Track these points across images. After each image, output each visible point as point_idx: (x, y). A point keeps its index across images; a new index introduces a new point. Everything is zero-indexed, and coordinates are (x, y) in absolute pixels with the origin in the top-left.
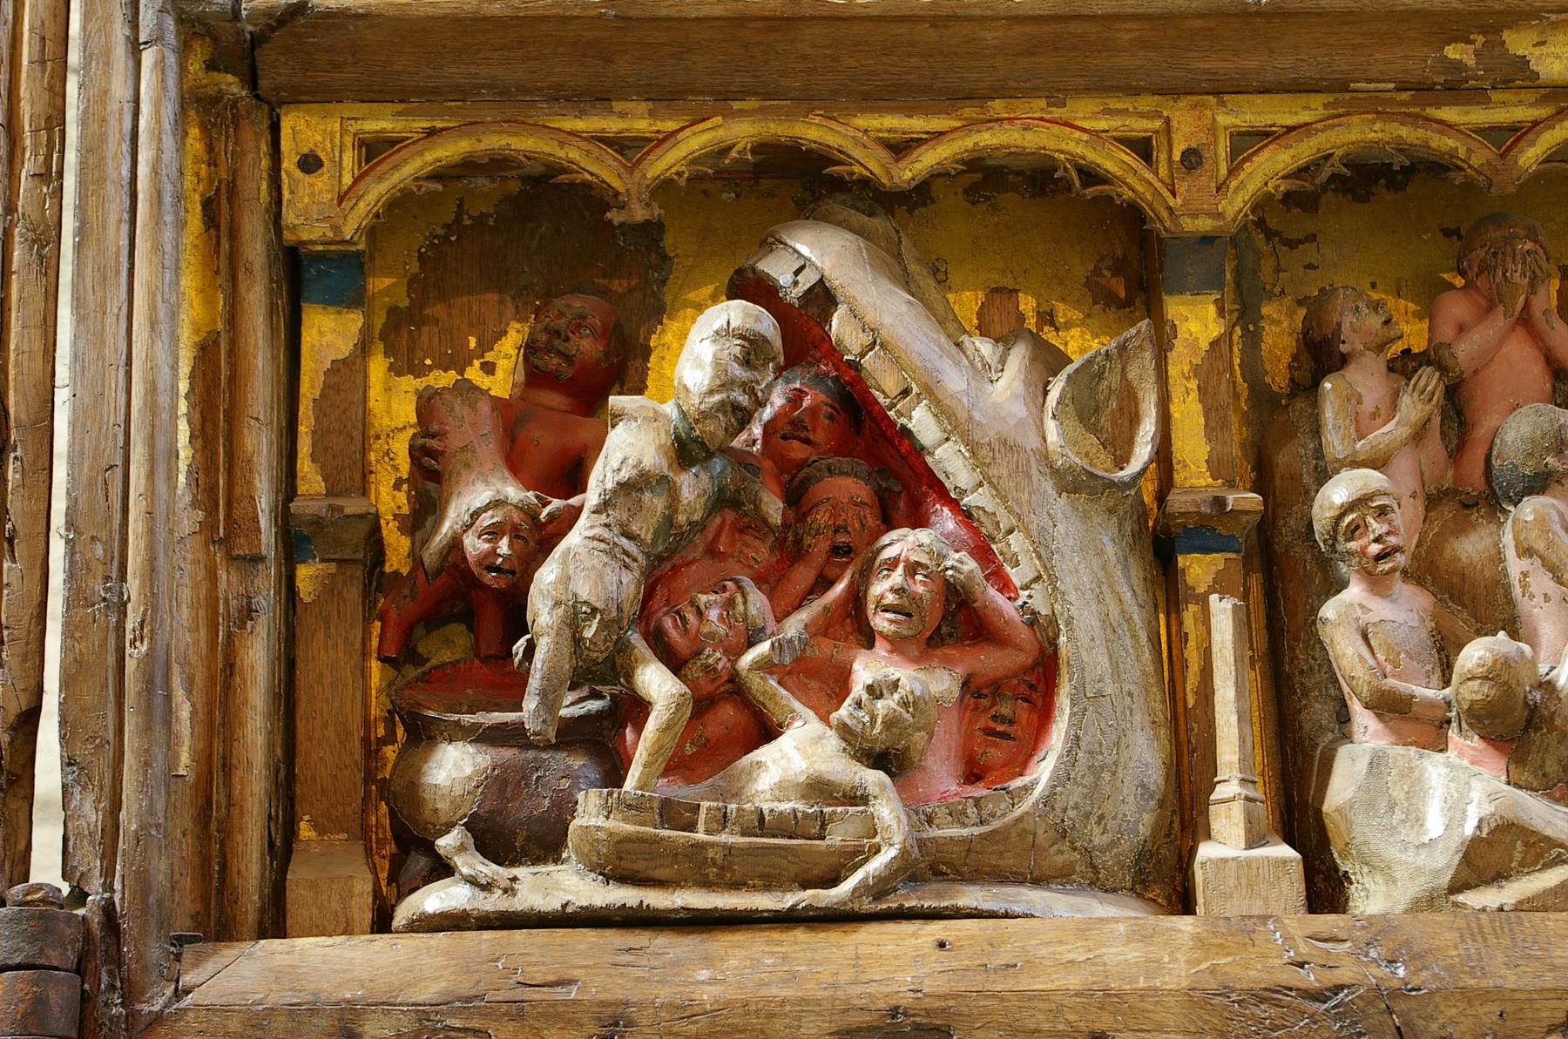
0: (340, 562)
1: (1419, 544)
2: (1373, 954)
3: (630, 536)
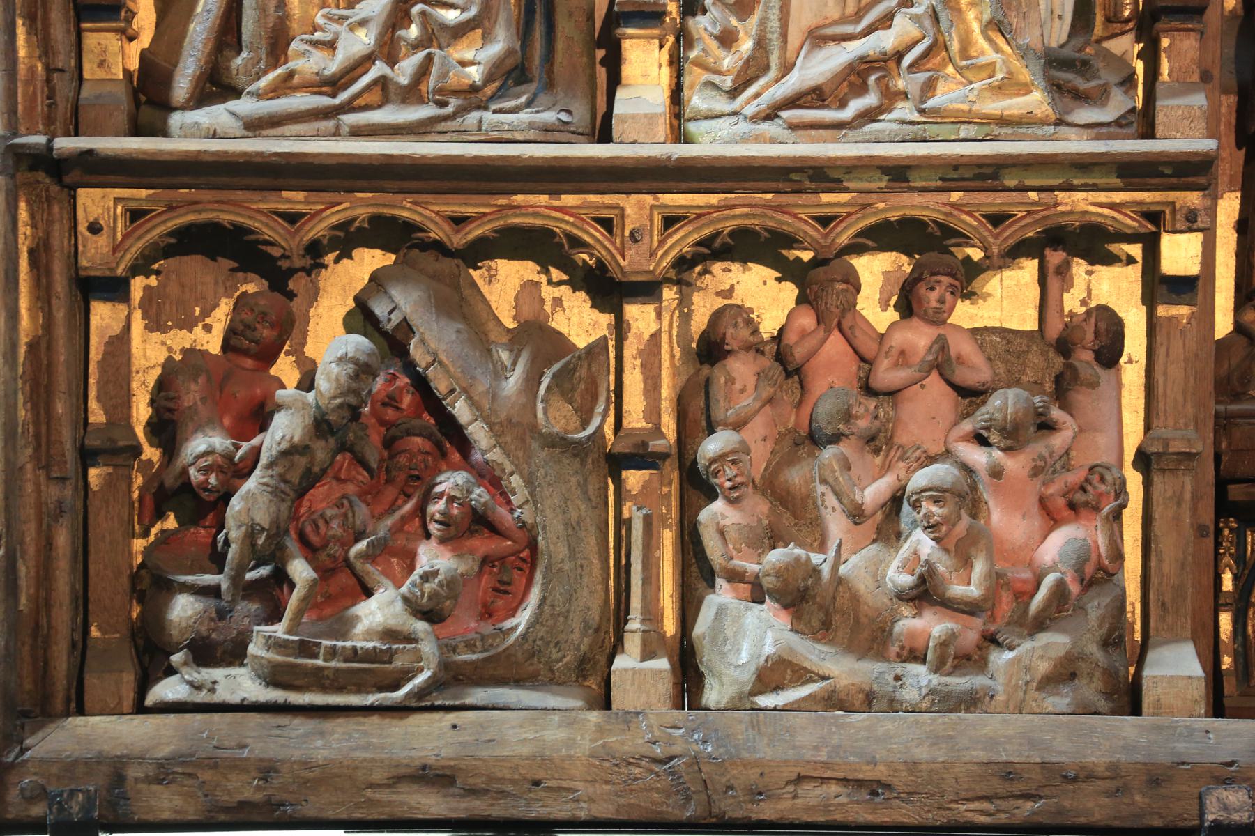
0: (115, 466)
1: (766, 469)
2: (696, 736)
3: (286, 482)
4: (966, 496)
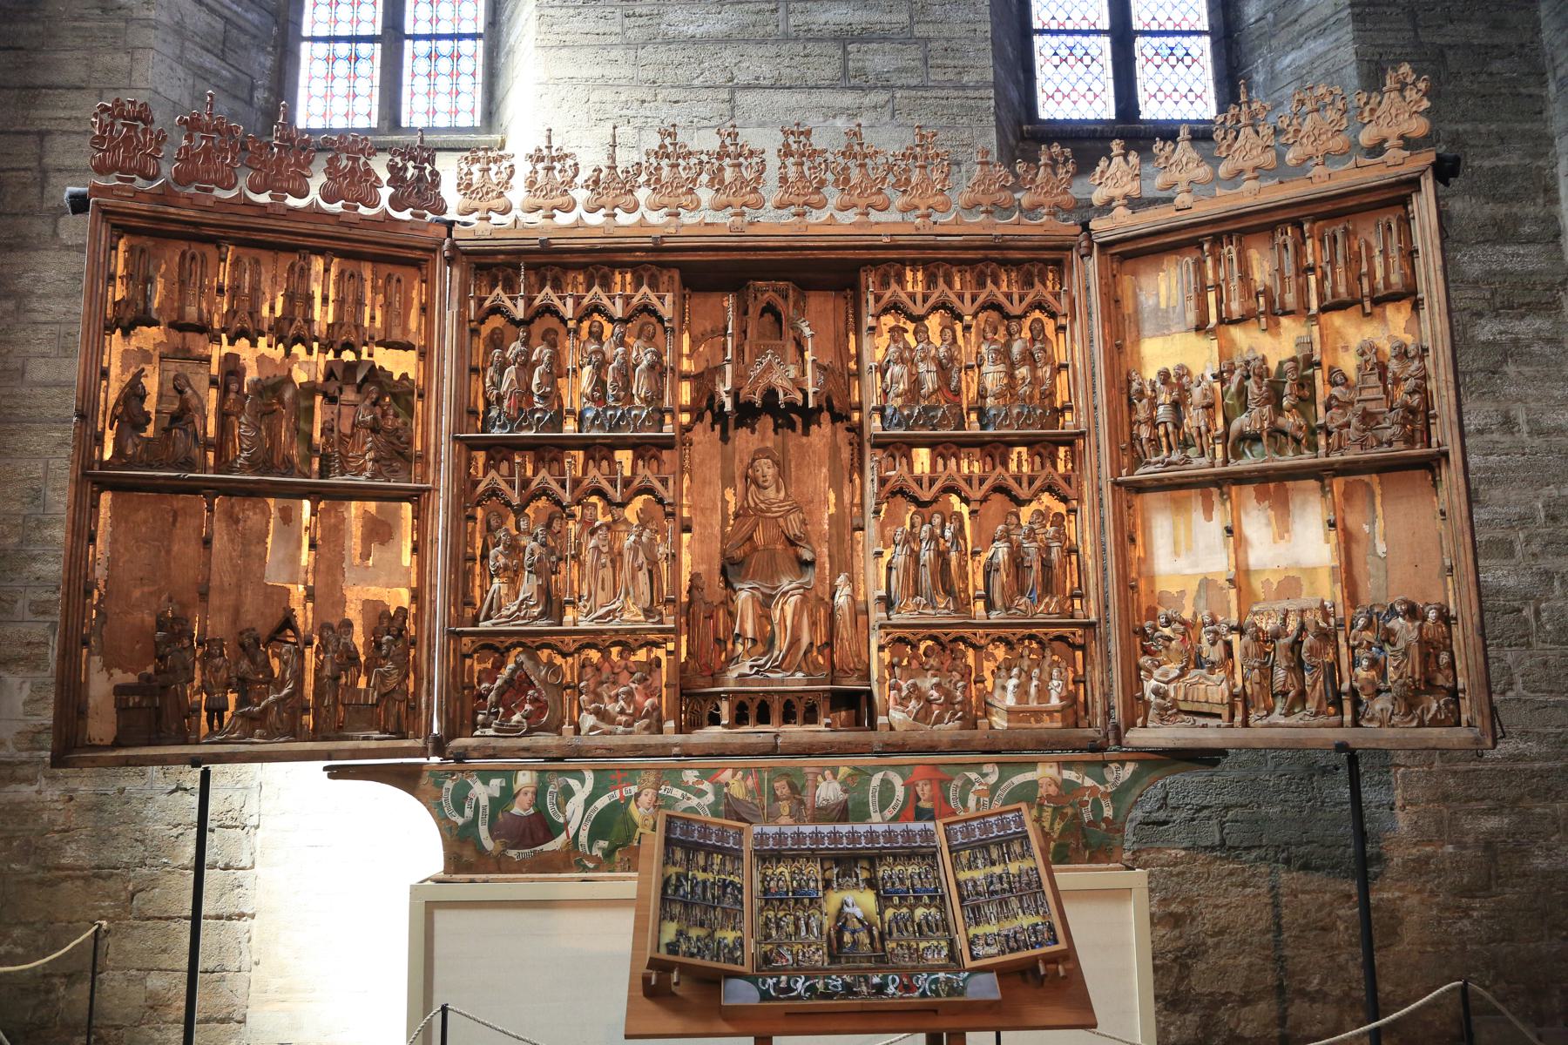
4: (630, 694)
